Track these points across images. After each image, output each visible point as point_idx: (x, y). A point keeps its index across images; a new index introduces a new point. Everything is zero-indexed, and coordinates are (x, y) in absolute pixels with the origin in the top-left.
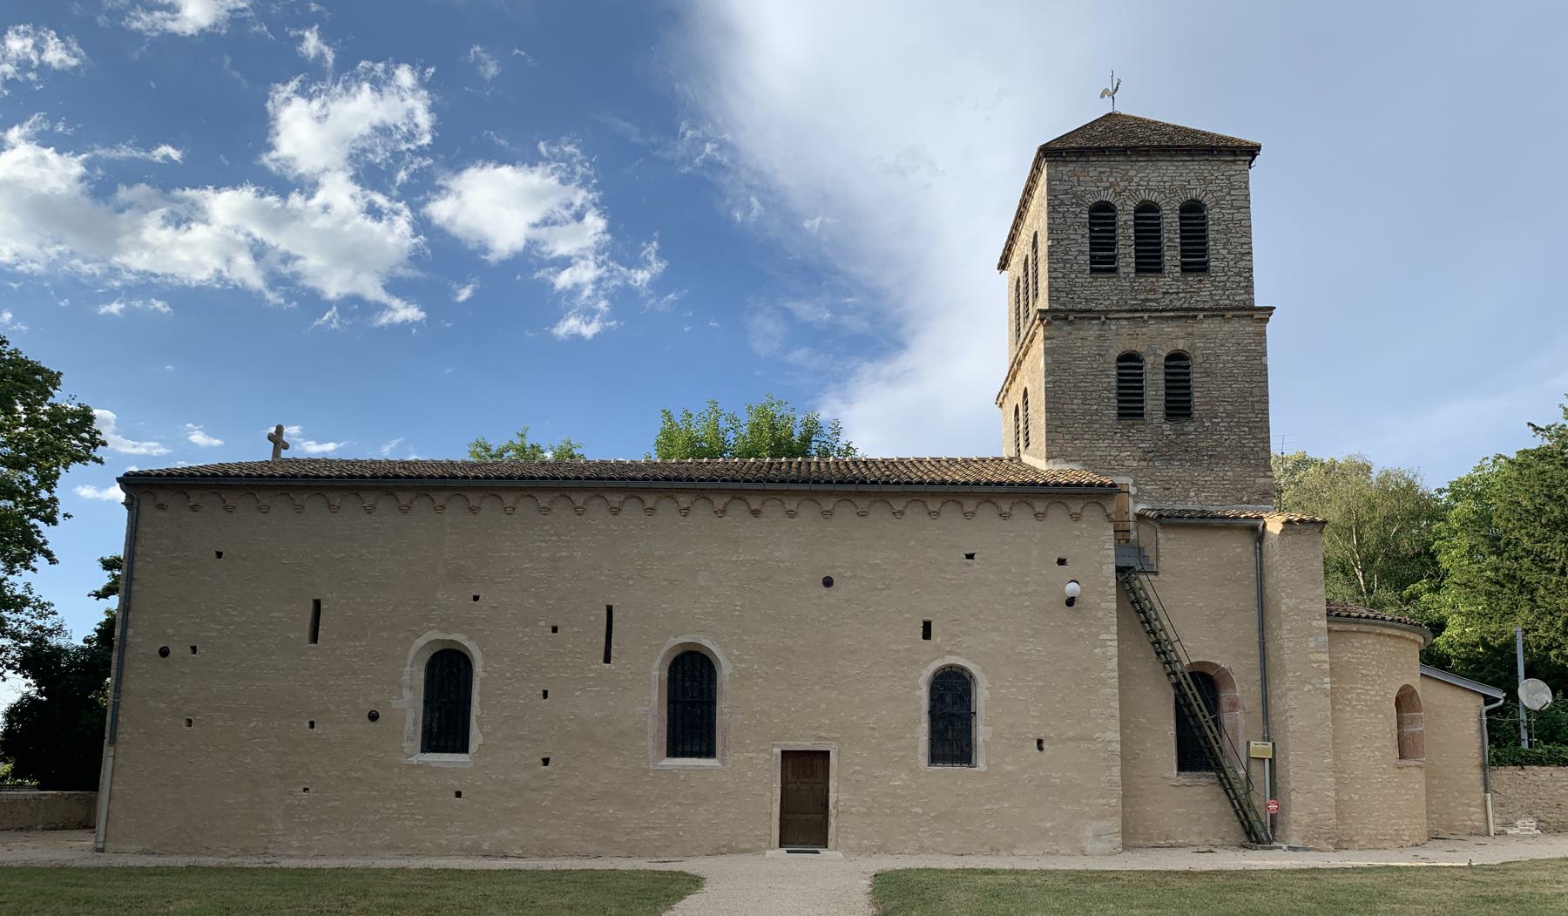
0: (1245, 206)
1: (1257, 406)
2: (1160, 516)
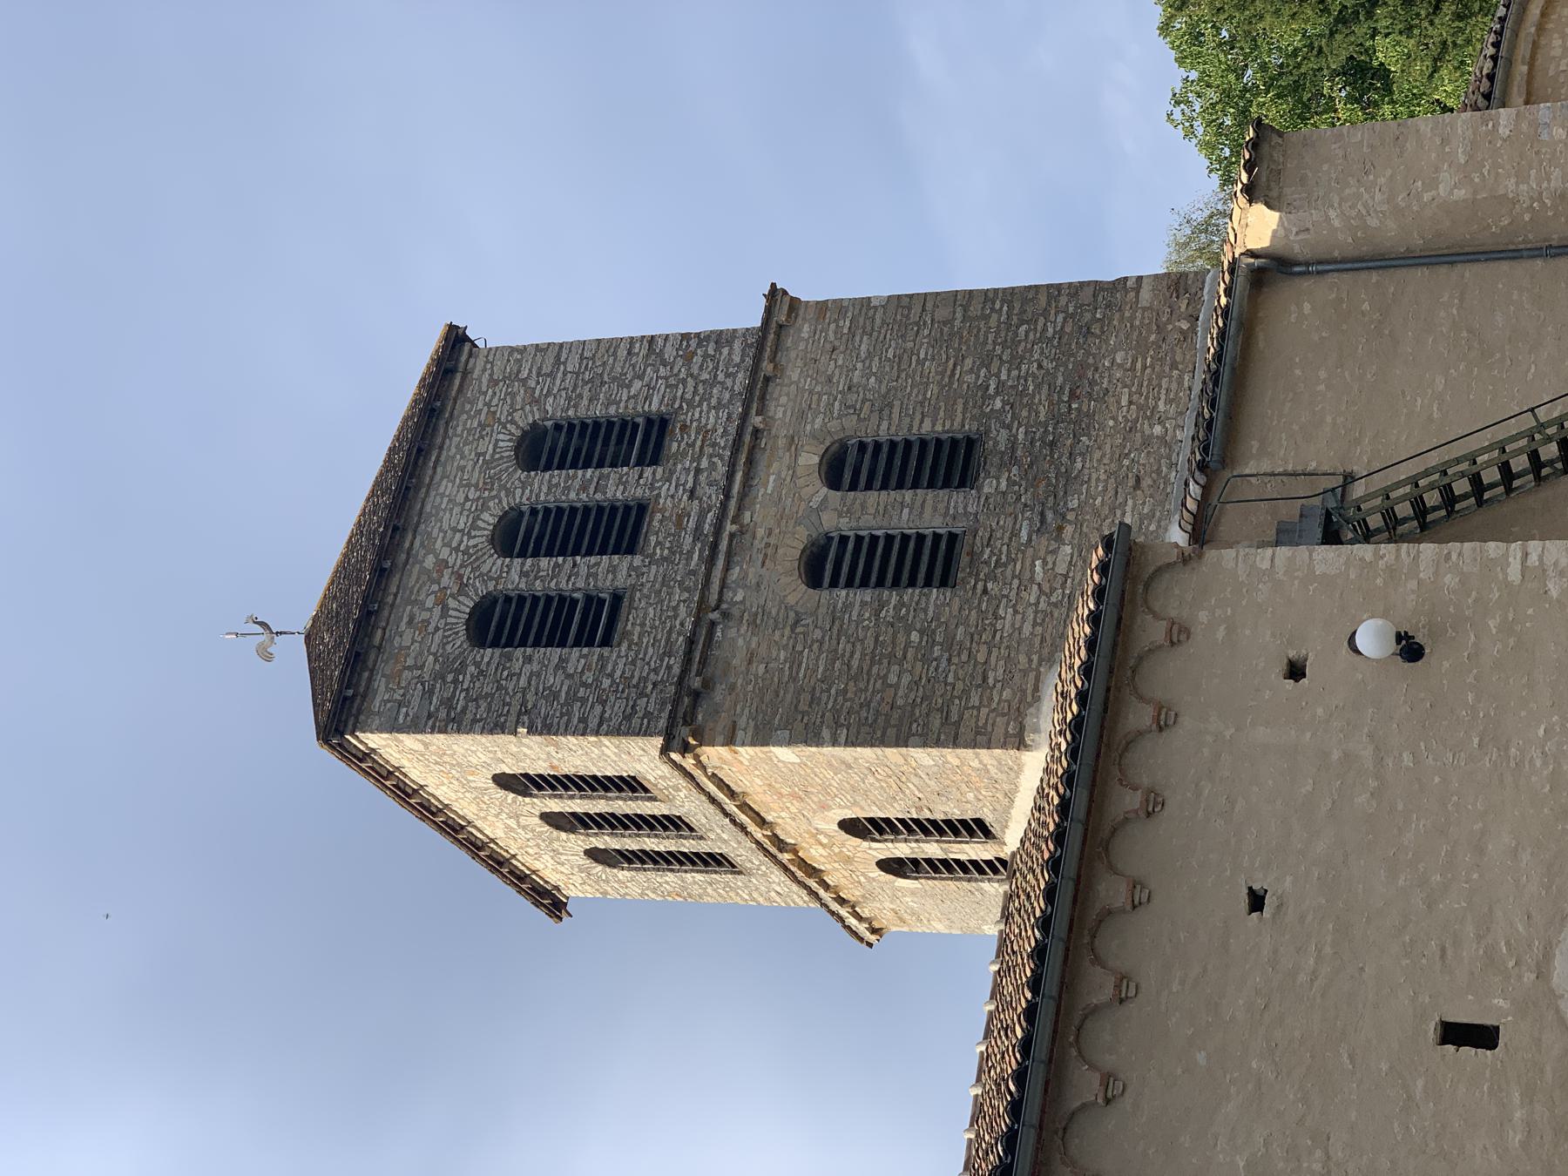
0: (557, 352)
1: (975, 309)
2: (1202, 467)
